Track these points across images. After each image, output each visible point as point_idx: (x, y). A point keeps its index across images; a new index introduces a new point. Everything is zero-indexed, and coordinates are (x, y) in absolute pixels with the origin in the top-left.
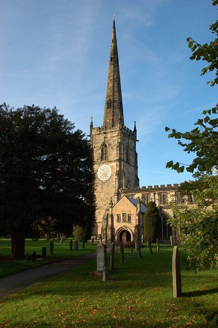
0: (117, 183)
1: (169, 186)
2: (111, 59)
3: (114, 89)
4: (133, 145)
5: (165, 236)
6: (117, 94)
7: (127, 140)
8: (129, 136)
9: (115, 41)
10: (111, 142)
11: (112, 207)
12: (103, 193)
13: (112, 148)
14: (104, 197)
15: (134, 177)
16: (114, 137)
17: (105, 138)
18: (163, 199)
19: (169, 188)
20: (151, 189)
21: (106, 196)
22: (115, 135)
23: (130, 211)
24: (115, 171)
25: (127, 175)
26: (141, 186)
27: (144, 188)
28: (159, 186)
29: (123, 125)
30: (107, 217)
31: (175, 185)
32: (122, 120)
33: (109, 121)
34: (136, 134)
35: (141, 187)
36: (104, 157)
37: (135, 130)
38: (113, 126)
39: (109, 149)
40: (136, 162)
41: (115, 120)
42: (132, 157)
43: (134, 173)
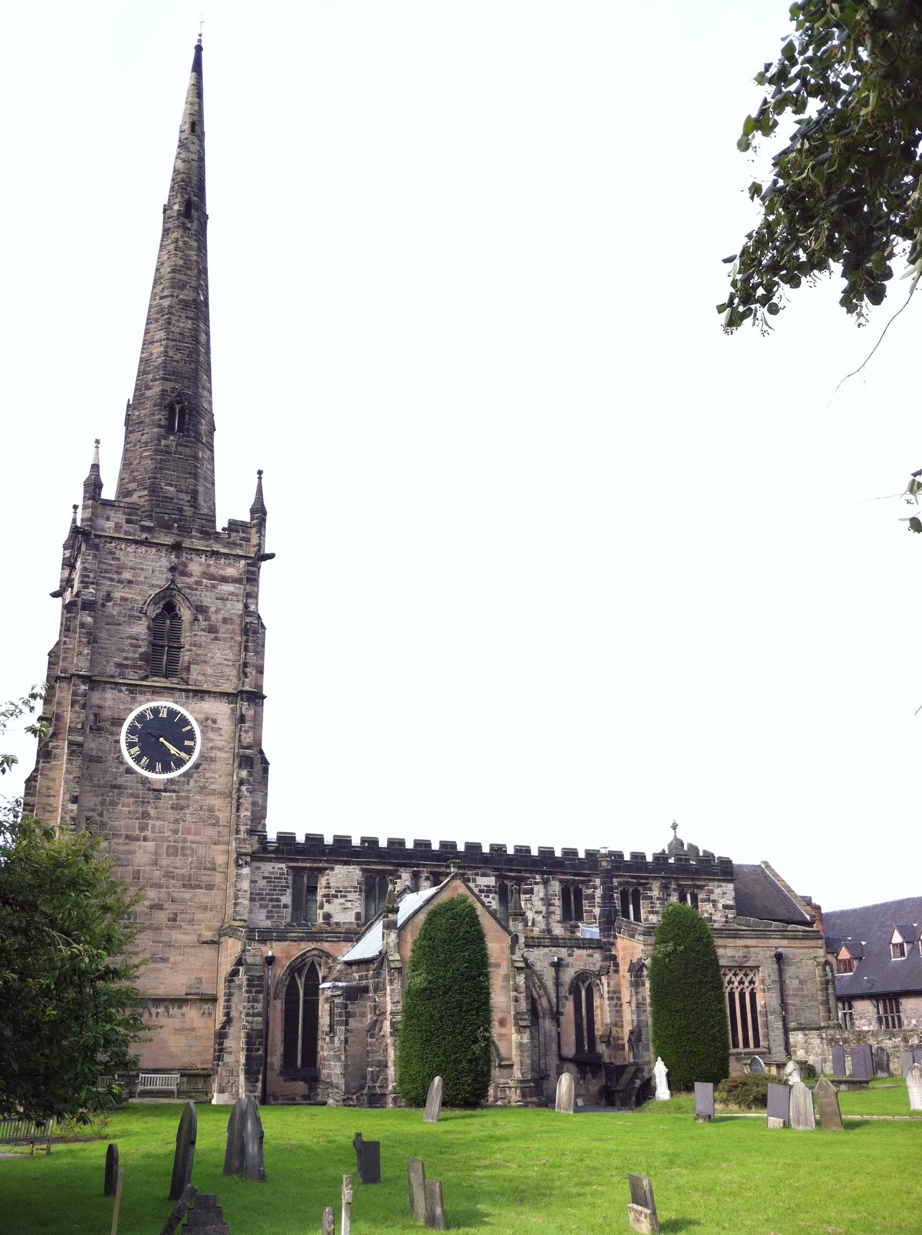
10: (207, 599)
12: (150, 845)
13: (212, 629)
14: (155, 863)
21: (165, 861)
22: (231, 572)
27: (286, 839)
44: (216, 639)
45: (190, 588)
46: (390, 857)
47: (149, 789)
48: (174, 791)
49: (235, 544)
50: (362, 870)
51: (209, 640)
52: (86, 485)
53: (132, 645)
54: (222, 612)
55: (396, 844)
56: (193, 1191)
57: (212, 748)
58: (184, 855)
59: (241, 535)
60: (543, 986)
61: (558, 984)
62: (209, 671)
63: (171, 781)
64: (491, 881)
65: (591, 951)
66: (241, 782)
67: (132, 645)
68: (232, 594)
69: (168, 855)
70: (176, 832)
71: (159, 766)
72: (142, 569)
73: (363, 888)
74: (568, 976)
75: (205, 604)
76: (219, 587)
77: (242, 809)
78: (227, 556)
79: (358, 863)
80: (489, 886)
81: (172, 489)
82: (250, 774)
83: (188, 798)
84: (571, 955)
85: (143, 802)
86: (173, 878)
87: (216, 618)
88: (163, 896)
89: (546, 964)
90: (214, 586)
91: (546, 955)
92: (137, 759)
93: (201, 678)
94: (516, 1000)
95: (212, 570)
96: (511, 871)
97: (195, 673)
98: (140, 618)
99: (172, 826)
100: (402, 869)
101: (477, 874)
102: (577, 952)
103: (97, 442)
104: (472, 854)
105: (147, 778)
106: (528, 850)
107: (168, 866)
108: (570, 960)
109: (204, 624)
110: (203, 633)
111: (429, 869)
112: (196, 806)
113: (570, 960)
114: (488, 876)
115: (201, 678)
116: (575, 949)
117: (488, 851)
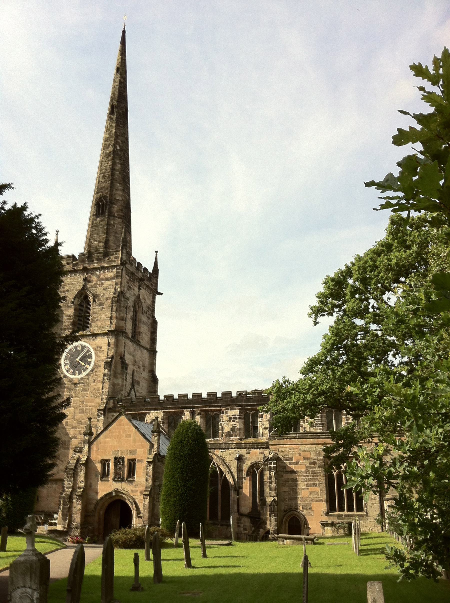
0: (107, 384)
1: (227, 395)
2: (118, 69)
3: (113, 175)
4: (149, 302)
5: (214, 515)
6: (120, 193)
7: (136, 289)
8: (141, 280)
9: (122, 70)
10: (99, 290)
11: (90, 443)
13: (101, 304)
15: (145, 374)
16: (106, 286)
17: (85, 279)
18: (212, 421)
19: (227, 400)
20: (184, 402)
21: (78, 416)
23: (134, 452)
24: (103, 357)
25: (130, 368)
26: (161, 394)
27: (169, 398)
28: (190, 396)
29: (129, 254)
30: (76, 467)
31: (209, 394)
32: (126, 244)
33: (99, 245)
34: (157, 277)
35: (162, 398)
36: (82, 321)
37: (156, 270)
38: (106, 254)
39: (94, 308)
40: (153, 340)
41: (111, 243)
42: (144, 329)
43: (147, 363)
44: (103, 308)
45: (92, 287)
46: (178, 404)
47: (72, 384)
48: (83, 383)
49: (112, 261)
50: (164, 412)
51: (100, 310)
53: (68, 319)
54: (106, 295)
55: (183, 397)
57: (99, 361)
58: (86, 413)
59: (115, 256)
61: (240, 470)
62: (99, 324)
63: (82, 379)
65: (262, 450)
67: (68, 319)
68: (110, 285)
69: (79, 413)
70: (83, 402)
71: (77, 372)
72: (73, 284)
73: (166, 421)
74: (246, 466)
75: (99, 293)
76: (105, 284)
77: (104, 388)
79: (162, 409)
80: (235, 415)
81: (96, 243)
83: (88, 385)
84: (248, 453)
85: (70, 390)
86: (81, 424)
87: (102, 299)
88: (77, 432)
89: (232, 459)
90: (102, 284)
91: (233, 453)
92: (68, 371)
93: (96, 328)
94: (147, 480)
95: (102, 276)
96: (249, 405)
98: (71, 306)
99: (82, 400)
100: (185, 410)
101: (228, 409)
102: (253, 451)
103: (57, 232)
104: (225, 398)
105: (72, 379)
107: (79, 419)
109: (98, 302)
110: (97, 307)
111: (200, 409)
112: (92, 389)
113: (248, 455)
114: (235, 410)
115: (96, 328)
116: (252, 449)
117: (177, 397)
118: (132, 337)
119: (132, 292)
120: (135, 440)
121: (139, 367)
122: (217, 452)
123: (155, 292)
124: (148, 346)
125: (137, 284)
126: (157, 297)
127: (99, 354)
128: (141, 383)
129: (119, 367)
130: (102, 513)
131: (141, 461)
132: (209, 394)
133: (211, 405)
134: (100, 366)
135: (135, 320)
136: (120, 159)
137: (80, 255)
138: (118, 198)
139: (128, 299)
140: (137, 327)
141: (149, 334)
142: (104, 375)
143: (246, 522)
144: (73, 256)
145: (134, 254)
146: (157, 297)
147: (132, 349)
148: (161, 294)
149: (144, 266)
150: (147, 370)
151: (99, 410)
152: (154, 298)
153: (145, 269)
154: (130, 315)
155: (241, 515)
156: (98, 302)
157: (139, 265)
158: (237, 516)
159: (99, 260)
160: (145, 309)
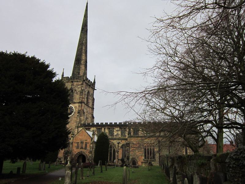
1: (115, 123)
4: (92, 92)
5: (110, 159)
7: (88, 88)
9: (86, 16)
10: (77, 89)
13: (77, 93)
15: (90, 116)
19: (116, 125)
20: (102, 125)
22: (80, 84)
24: (77, 110)
25: (86, 114)
27: (98, 124)
37: (94, 82)
40: (93, 105)
42: (90, 101)
43: (91, 112)
52: (62, 75)
56: (59, 157)
60: (116, 147)
64: (119, 129)
66: (78, 116)
74: (120, 145)
78: (79, 81)
82: (79, 114)
84: (121, 141)
87: (77, 91)
97: (74, 100)
102: (123, 141)
106: (112, 123)
108: (121, 142)
118: (87, 104)
119: (87, 89)
120: (87, 137)
121: (88, 113)
122: (112, 141)
123: (94, 89)
124: (91, 107)
125: (88, 87)
126: (95, 90)
127: (76, 109)
128: (89, 118)
129: (82, 113)
130: (77, 158)
131: (89, 143)
132: (101, 123)
133: (111, 126)
134: (76, 113)
135: (87, 98)
136: (84, 46)
137: (71, 77)
138: (83, 58)
139: (85, 92)
140: (88, 101)
141: (92, 103)
142: (78, 116)
143: (120, 162)
144: (68, 77)
145: (88, 77)
146: (95, 90)
147: (86, 108)
148: (96, 90)
149: (91, 81)
150: (91, 114)
151: (76, 127)
152: (94, 91)
153: (91, 82)
154: (86, 96)
155: (118, 160)
156: (75, 92)
157: (89, 80)
158: (117, 160)
159: (77, 79)
160: (91, 94)
